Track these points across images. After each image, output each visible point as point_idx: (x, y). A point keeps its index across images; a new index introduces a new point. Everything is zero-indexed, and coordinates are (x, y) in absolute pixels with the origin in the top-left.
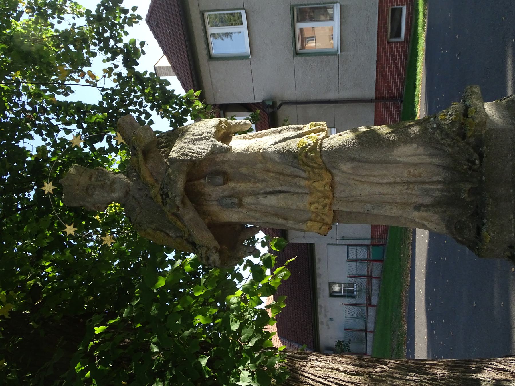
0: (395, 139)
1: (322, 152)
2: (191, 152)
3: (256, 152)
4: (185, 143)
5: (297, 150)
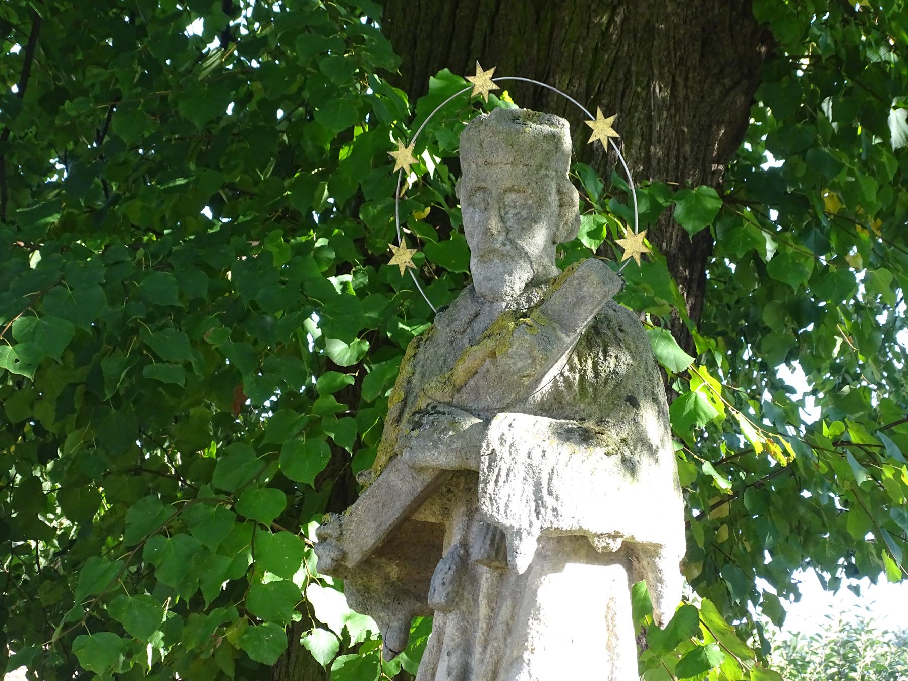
2: (499, 475)
3: (527, 641)
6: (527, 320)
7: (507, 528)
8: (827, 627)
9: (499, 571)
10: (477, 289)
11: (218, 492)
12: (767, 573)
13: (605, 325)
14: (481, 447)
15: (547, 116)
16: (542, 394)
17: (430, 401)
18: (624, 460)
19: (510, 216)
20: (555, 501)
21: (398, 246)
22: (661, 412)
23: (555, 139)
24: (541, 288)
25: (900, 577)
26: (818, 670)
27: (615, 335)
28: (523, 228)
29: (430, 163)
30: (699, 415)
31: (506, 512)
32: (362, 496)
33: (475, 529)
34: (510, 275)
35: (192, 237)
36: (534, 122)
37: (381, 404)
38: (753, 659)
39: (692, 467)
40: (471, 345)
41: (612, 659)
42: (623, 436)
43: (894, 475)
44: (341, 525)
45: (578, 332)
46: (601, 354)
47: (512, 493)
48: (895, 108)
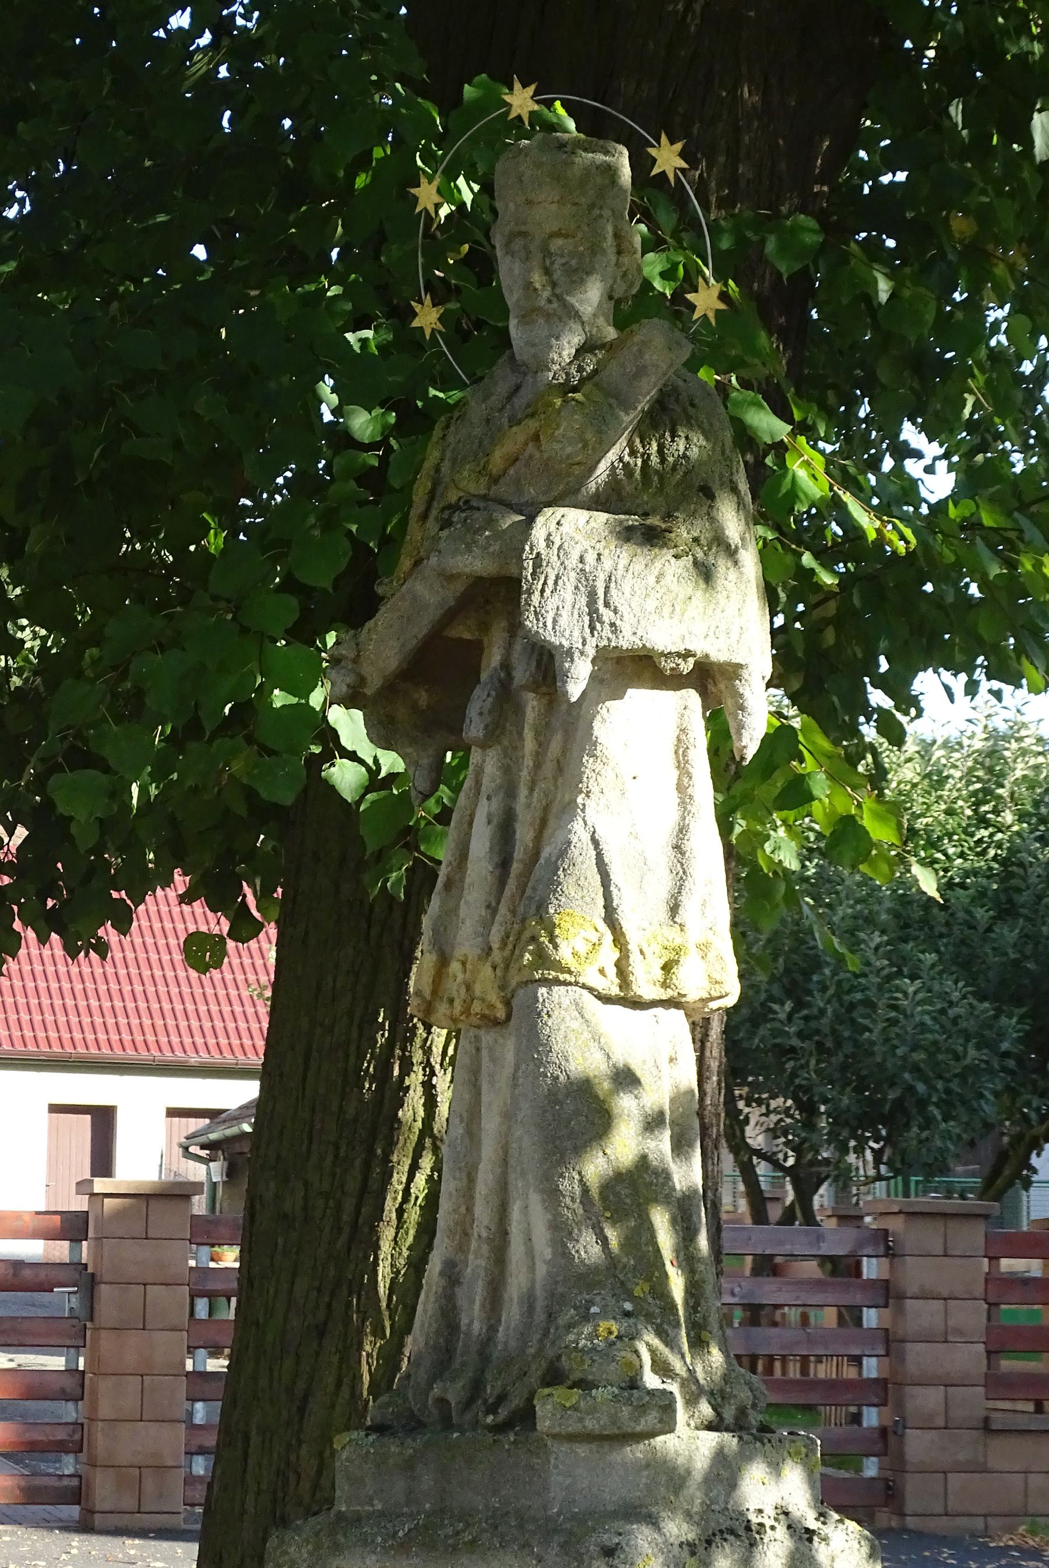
0: (564, 1196)
1: (535, 984)
2: (545, 583)
4: (582, 560)
5: (552, 911)
6: (578, 396)
7: (556, 647)
8: (968, 734)
9: (547, 697)
10: (518, 357)
11: (215, 598)
12: (882, 683)
13: (672, 399)
14: (523, 550)
15: (601, 142)
16: (596, 483)
17: (462, 494)
18: (696, 563)
19: (556, 266)
20: (612, 614)
21: (422, 304)
22: (740, 504)
23: (610, 172)
24: (596, 355)
25: (1042, 687)
26: (959, 785)
27: (685, 410)
28: (573, 282)
29: (467, 191)
30: (798, 497)
31: (554, 628)
32: (383, 609)
33: (518, 647)
34: (557, 338)
35: (178, 286)
36: (586, 150)
37: (406, 492)
38: (866, 787)
39: (789, 559)
40: (511, 427)
41: (683, 803)
42: (696, 535)
43: (1033, 566)
44: (357, 645)
45: (639, 408)
46: (667, 434)
47: (560, 604)
48: (1040, 111)
